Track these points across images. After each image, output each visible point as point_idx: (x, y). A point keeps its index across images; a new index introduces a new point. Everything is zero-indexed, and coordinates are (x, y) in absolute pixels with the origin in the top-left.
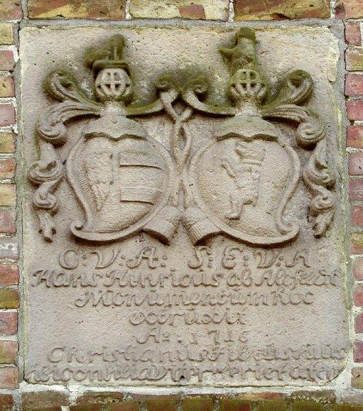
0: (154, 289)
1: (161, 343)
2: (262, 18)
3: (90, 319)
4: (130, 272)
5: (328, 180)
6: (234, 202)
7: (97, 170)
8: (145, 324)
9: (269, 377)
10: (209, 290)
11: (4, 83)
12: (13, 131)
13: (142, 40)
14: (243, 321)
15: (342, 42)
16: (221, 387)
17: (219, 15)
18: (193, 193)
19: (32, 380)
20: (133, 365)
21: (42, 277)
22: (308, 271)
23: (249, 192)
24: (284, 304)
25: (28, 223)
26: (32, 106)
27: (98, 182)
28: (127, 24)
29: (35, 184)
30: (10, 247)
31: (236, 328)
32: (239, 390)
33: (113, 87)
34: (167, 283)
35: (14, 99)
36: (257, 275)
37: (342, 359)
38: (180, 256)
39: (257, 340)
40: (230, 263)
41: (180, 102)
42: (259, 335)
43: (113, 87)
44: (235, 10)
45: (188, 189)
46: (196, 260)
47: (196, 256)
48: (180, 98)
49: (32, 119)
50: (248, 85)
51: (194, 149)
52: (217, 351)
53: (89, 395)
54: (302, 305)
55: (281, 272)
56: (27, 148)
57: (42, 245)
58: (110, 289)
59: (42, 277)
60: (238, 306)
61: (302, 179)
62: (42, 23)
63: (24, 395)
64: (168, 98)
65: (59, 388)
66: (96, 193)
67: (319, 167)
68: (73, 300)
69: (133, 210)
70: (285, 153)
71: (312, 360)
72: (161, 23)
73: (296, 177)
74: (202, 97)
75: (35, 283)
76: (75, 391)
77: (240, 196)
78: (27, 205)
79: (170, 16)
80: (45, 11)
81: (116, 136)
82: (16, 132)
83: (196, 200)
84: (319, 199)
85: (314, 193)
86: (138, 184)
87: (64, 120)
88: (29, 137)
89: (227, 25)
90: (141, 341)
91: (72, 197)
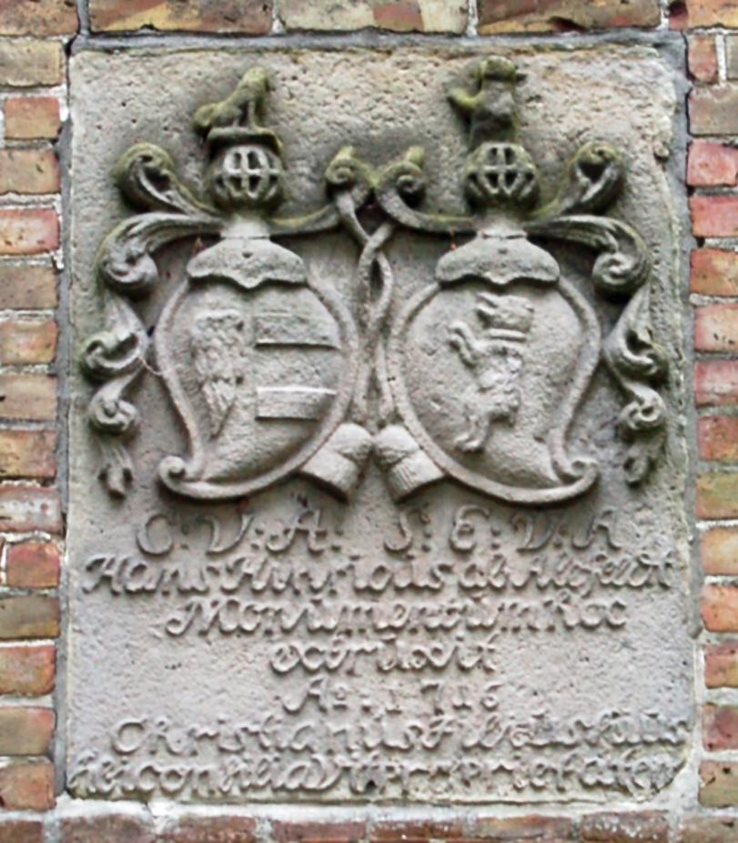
0: (318, 597)
1: (331, 712)
2: (531, 28)
3: (194, 660)
4: (275, 564)
5: (653, 371)
6: (473, 418)
7: (214, 355)
8: (299, 672)
9: (539, 782)
10: (421, 602)
11: (39, 163)
12: (54, 263)
13: (301, 76)
14: (489, 663)
15: (681, 76)
16: (445, 804)
17: (448, 23)
18: (395, 393)
19: (81, 791)
20: (277, 760)
21: (102, 577)
22: (615, 560)
23: (500, 398)
24: (569, 628)
25: (79, 458)
26: (90, 217)
27: (216, 379)
28: (274, 42)
29: (96, 378)
30: (44, 507)
31: (478, 681)
32: (483, 813)
33: (245, 184)
34: (342, 586)
35: (58, 197)
36: (518, 570)
37: (680, 743)
38: (368, 535)
39: (517, 709)
40: (464, 544)
41: (372, 211)
42: (522, 692)
43: (245, 184)
44: (479, 11)
45: (385, 387)
46: (399, 536)
47: (399, 525)
48: (370, 220)
49: (91, 240)
50: (501, 178)
51: (399, 301)
52: (438, 729)
53: (187, 823)
54: (603, 629)
55: (565, 562)
56: (79, 296)
57: (103, 504)
58: (235, 598)
59: (102, 577)
60: (480, 633)
61: (602, 365)
62: (115, 43)
63: (65, 822)
64: (347, 204)
65: (131, 809)
66: (210, 401)
67: (634, 343)
68: (162, 620)
69: (278, 437)
70: (572, 313)
71: (626, 748)
72: (337, 42)
73: (588, 366)
74: (414, 200)
75: (89, 584)
76: (163, 813)
77: (486, 405)
78: (76, 422)
79: (354, 26)
80: (122, 17)
81: (250, 283)
82: (60, 266)
83: (401, 412)
84: (634, 412)
85: (627, 397)
86: (286, 388)
87: (152, 249)
88: (87, 278)
89: (465, 44)
90: (292, 707)
91: (162, 404)
